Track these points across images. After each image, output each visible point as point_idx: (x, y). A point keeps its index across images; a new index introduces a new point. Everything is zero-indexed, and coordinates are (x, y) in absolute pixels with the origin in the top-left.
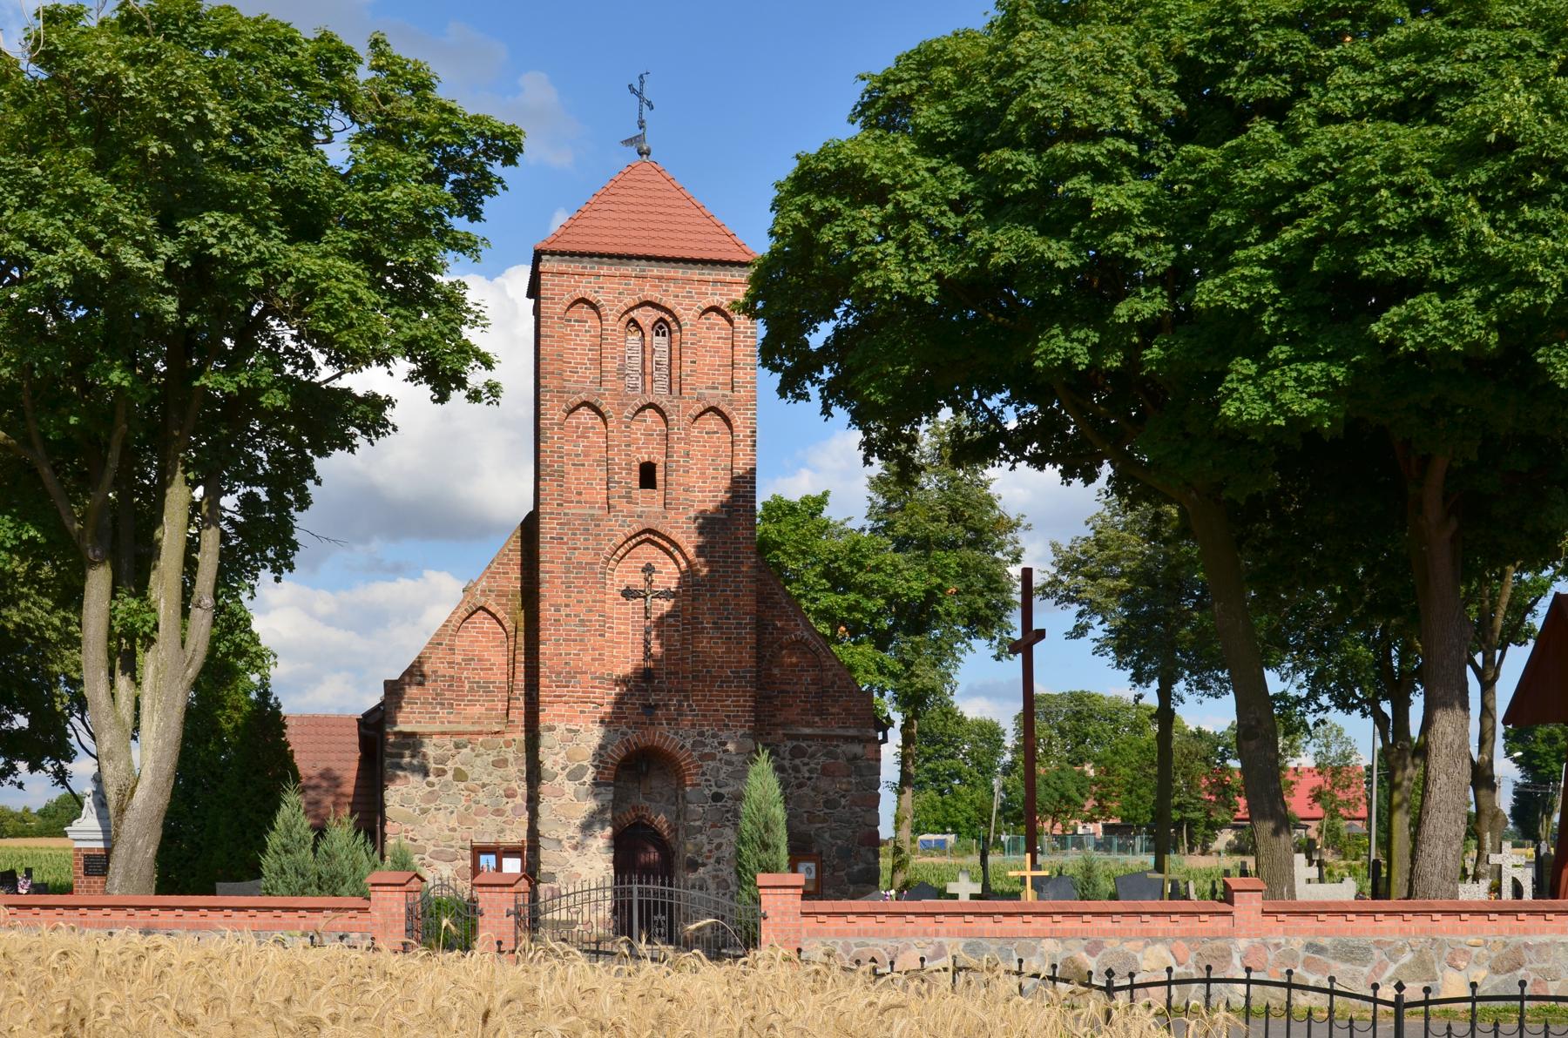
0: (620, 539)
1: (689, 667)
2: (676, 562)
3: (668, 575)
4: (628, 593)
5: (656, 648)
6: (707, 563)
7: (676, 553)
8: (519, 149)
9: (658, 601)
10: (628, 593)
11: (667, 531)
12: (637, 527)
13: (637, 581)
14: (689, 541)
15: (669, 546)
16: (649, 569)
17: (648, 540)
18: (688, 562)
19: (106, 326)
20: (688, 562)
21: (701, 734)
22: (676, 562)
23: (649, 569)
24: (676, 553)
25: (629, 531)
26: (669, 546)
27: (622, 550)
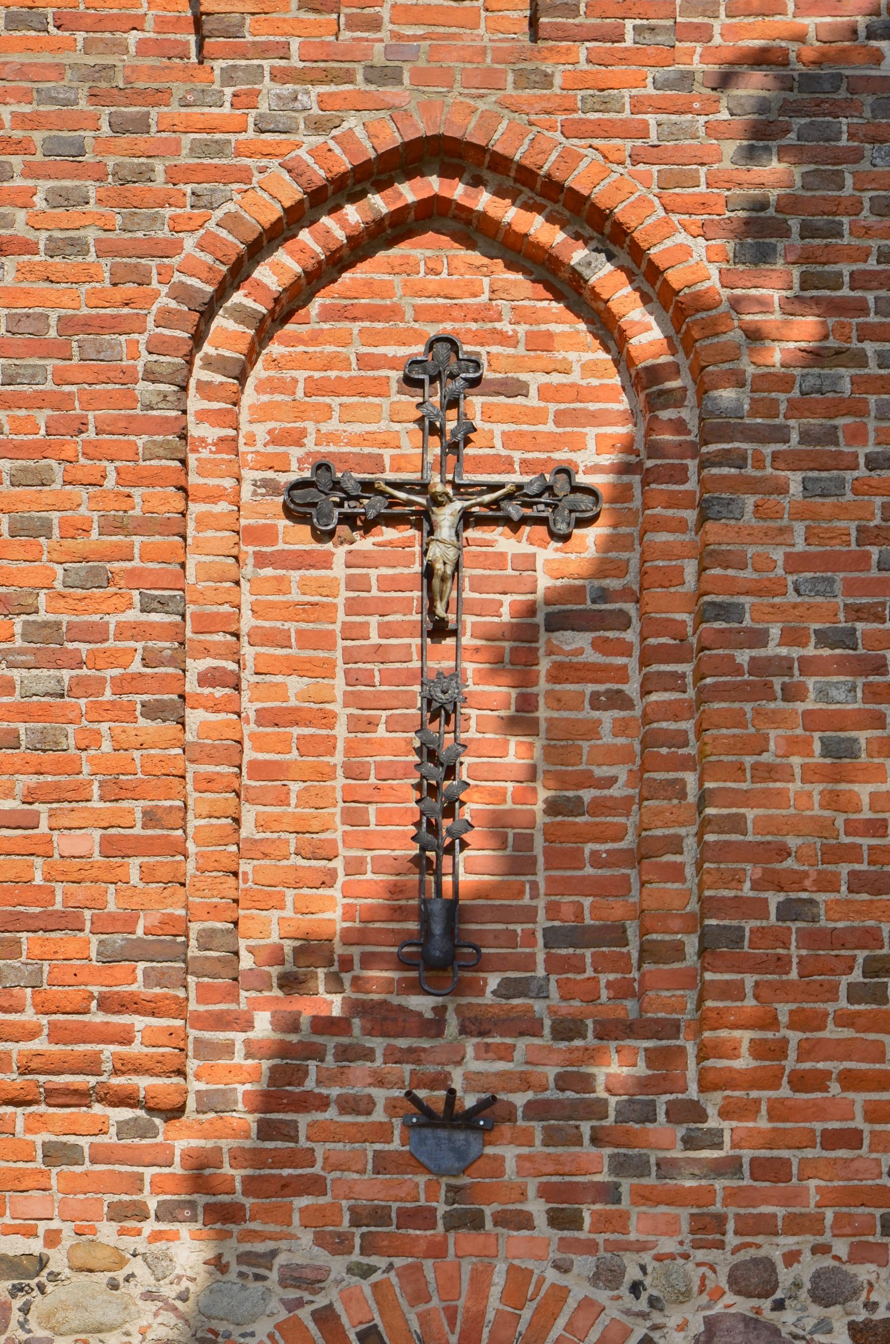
0: (270, 195)
1: (679, 894)
2: (608, 330)
3: (562, 399)
4: (328, 502)
5: (497, 768)
6: (813, 290)
7: (603, 274)
8: (886, 665)
9: (501, 540)
10: (328, 502)
11: (505, 138)
12: (367, 134)
13: (386, 437)
14: (685, 189)
15: (561, 240)
16: (443, 372)
17: (431, 215)
18: (679, 310)
19: (671, 391)
20: (679, 310)
21: (755, 1280)
22: (608, 330)
23: (443, 372)
24: (603, 274)
25: (321, 155)
26: (561, 240)
27: (274, 273)
